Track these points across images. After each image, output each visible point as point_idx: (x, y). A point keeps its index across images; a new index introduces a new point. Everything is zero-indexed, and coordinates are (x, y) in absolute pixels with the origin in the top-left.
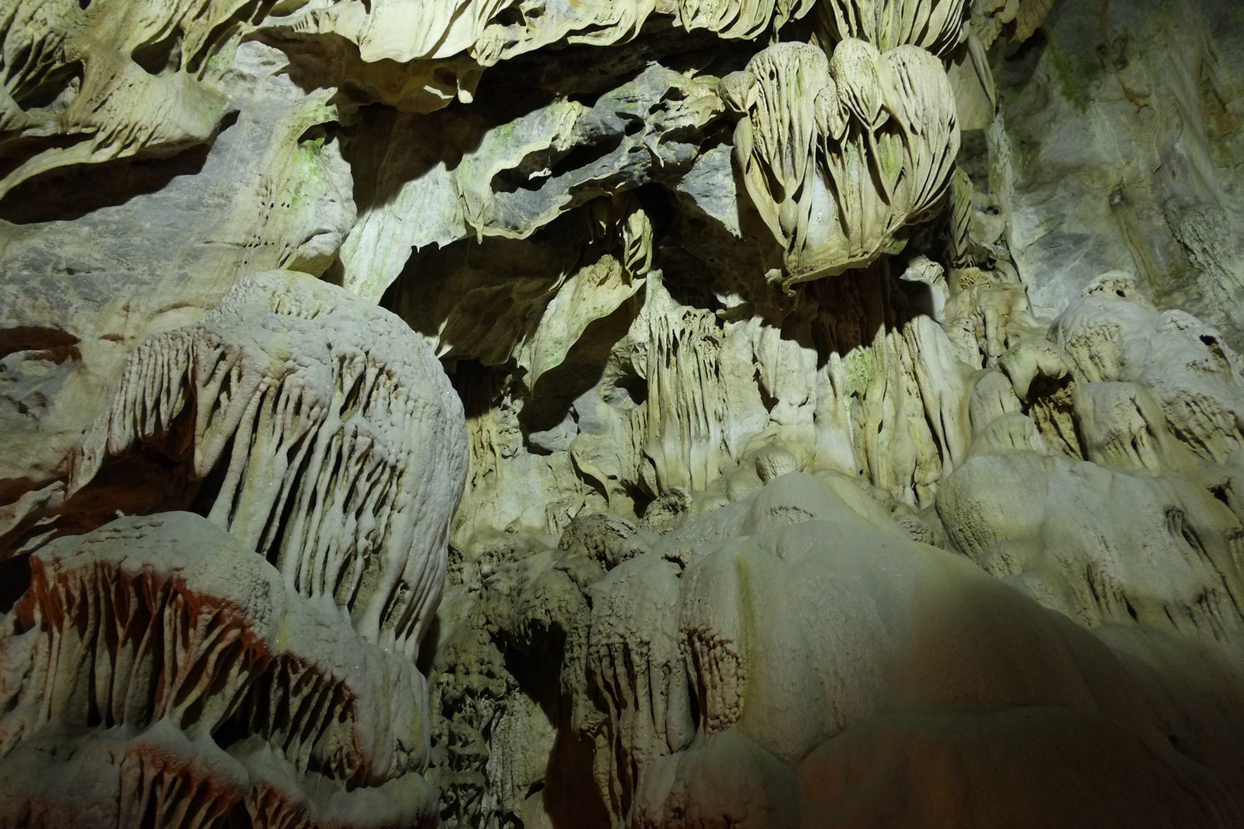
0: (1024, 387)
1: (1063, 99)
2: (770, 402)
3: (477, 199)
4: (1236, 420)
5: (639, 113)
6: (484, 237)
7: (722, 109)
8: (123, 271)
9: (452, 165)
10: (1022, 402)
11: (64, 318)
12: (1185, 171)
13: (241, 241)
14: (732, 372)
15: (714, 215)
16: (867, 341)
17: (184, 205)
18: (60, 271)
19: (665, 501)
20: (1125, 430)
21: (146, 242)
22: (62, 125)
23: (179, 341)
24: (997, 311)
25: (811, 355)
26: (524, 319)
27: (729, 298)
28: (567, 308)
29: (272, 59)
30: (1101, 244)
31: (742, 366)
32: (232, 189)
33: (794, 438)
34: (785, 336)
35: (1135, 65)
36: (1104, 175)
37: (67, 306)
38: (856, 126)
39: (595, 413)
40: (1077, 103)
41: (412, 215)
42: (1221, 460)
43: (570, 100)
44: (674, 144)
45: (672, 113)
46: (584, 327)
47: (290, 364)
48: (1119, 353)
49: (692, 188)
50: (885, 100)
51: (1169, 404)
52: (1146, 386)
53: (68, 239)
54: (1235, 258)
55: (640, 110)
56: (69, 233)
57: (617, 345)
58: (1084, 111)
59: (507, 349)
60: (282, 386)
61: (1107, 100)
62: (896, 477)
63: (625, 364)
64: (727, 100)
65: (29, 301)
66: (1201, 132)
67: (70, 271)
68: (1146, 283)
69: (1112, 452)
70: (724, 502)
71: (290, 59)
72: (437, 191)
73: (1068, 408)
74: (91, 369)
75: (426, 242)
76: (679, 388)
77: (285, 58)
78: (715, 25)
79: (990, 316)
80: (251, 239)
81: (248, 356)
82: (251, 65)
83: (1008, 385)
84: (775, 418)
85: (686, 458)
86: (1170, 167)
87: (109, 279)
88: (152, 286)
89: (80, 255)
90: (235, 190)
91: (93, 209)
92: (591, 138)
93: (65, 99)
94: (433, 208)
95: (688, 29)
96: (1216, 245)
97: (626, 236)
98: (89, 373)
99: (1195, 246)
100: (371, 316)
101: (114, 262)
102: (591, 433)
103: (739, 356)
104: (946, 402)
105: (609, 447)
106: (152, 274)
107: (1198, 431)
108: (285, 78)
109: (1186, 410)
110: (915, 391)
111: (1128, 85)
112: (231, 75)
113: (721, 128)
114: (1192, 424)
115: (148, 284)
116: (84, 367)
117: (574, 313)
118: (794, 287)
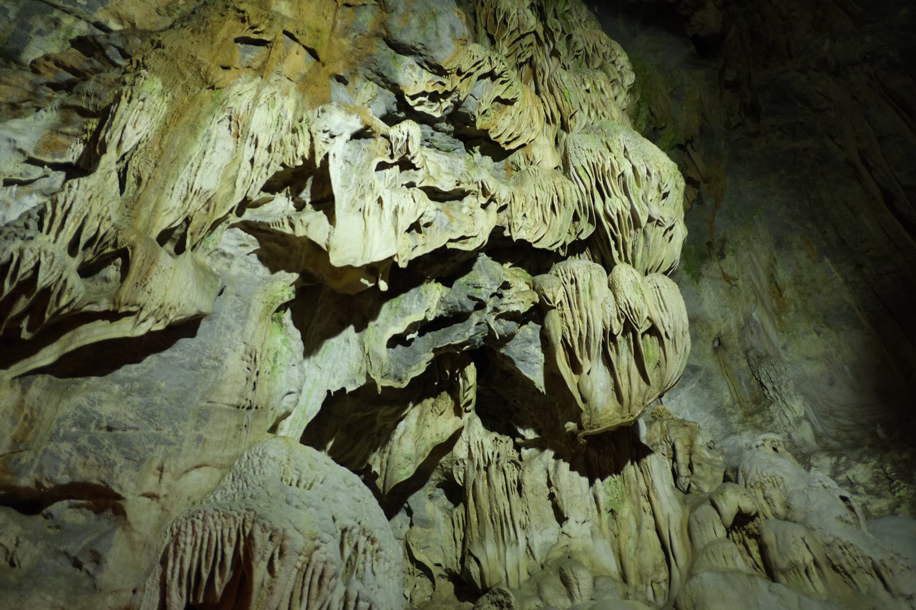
0: (729, 520)
1: (684, 272)
2: (561, 517)
3: (379, 358)
4: (873, 563)
5: (484, 297)
6: (382, 387)
7: (537, 301)
8: (153, 431)
9: (361, 327)
10: (727, 530)
11: (110, 476)
12: (758, 331)
13: (235, 403)
14: (532, 491)
15: (527, 375)
16: (618, 470)
17: (188, 366)
18: (101, 428)
19: (494, 598)
20: (801, 562)
21: (165, 402)
22: (114, 303)
23: (231, 521)
24: (683, 442)
25: (585, 480)
26: (379, 435)
27: (527, 431)
28: (413, 428)
29: (247, 242)
30: (709, 374)
31: (539, 487)
32: (226, 355)
33: (580, 549)
34: (572, 469)
35: (730, 258)
36: (709, 327)
37: (113, 465)
38: (629, 327)
39: (425, 511)
40: (693, 277)
41: (329, 365)
42: (864, 590)
43: (436, 282)
44: (503, 321)
45: (505, 300)
46: (430, 449)
47: (317, 542)
48: (785, 498)
49: (513, 354)
50: (650, 313)
51: (828, 545)
52: (810, 529)
53: (104, 396)
54: (794, 397)
55: (483, 294)
56: (104, 391)
57: (444, 458)
58: (697, 282)
59: (367, 457)
60: (310, 561)
61: (712, 278)
62: (641, 578)
63: (447, 473)
64: (542, 296)
65: (81, 459)
66: (770, 310)
67: (109, 429)
68: (737, 405)
69: (792, 576)
70: (539, 603)
71: (260, 244)
72: (348, 348)
73: (758, 537)
74: (135, 527)
75: (338, 388)
76: (492, 499)
77: (257, 243)
78: (530, 238)
79: (679, 446)
80: (244, 402)
81: (289, 538)
82: (231, 246)
83: (718, 517)
84: (566, 531)
85: (502, 559)
86: (750, 328)
87: (144, 439)
88: (178, 446)
89: (117, 414)
90: (226, 355)
91: (118, 366)
92: (450, 312)
93: (108, 275)
94: (345, 361)
95: (515, 239)
96: (782, 387)
97: (461, 381)
98: (133, 530)
99: (768, 385)
100: (349, 483)
101: (146, 422)
102: (421, 526)
103: (537, 479)
104: (672, 521)
105: (436, 540)
106: (176, 435)
107: (847, 567)
108: (254, 258)
109: (839, 552)
110: (649, 510)
111: (725, 270)
112: (216, 253)
113: (539, 312)
114: (843, 562)
115: (174, 444)
116: (129, 524)
117: (419, 436)
118: (585, 437)
